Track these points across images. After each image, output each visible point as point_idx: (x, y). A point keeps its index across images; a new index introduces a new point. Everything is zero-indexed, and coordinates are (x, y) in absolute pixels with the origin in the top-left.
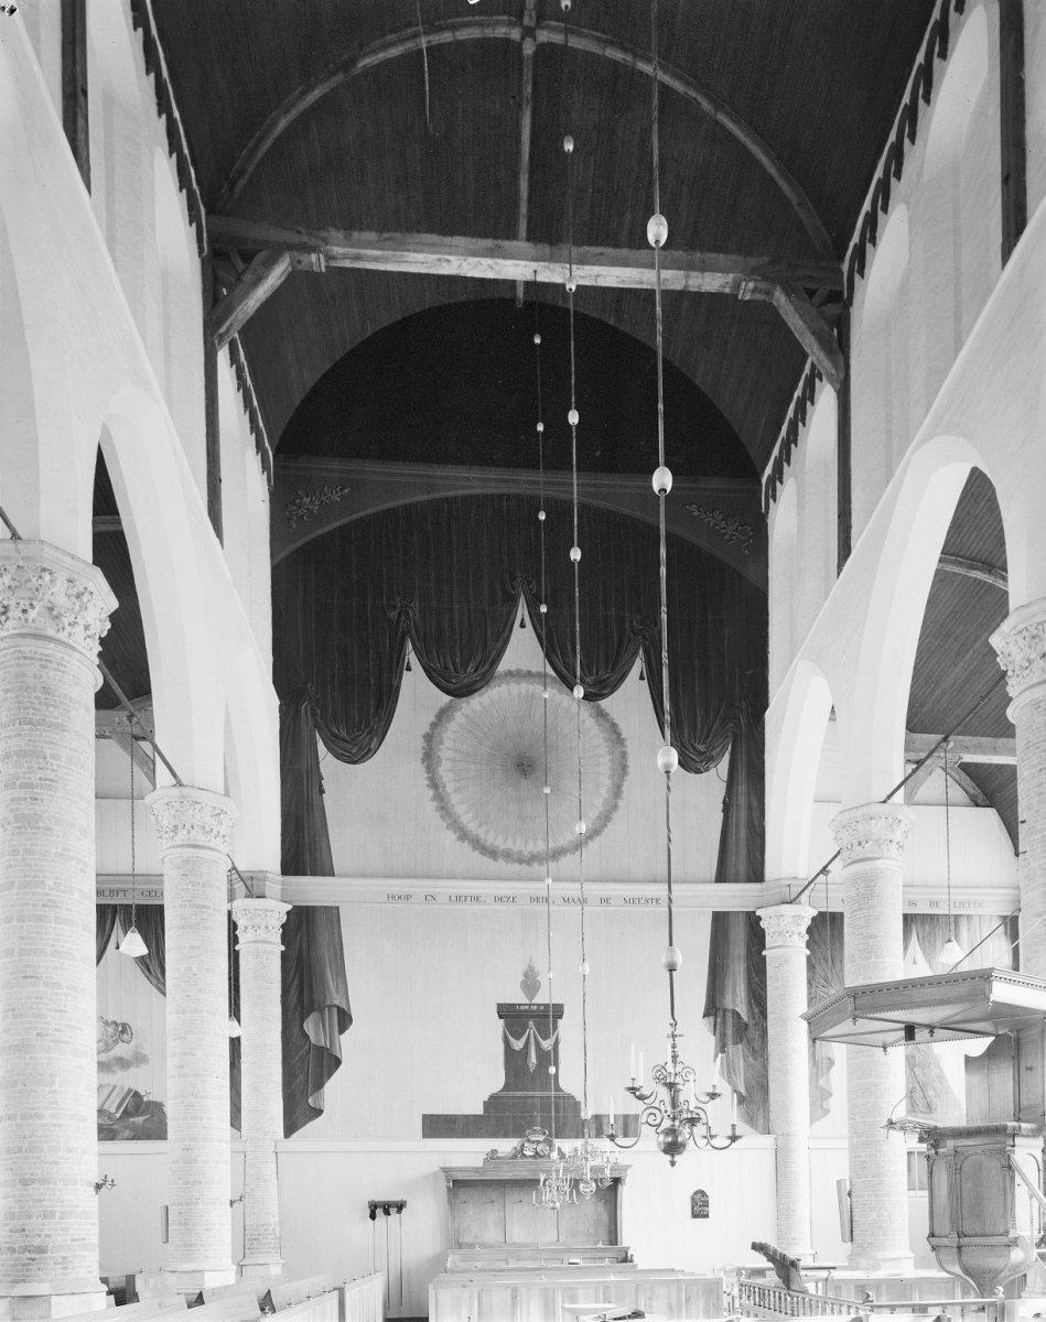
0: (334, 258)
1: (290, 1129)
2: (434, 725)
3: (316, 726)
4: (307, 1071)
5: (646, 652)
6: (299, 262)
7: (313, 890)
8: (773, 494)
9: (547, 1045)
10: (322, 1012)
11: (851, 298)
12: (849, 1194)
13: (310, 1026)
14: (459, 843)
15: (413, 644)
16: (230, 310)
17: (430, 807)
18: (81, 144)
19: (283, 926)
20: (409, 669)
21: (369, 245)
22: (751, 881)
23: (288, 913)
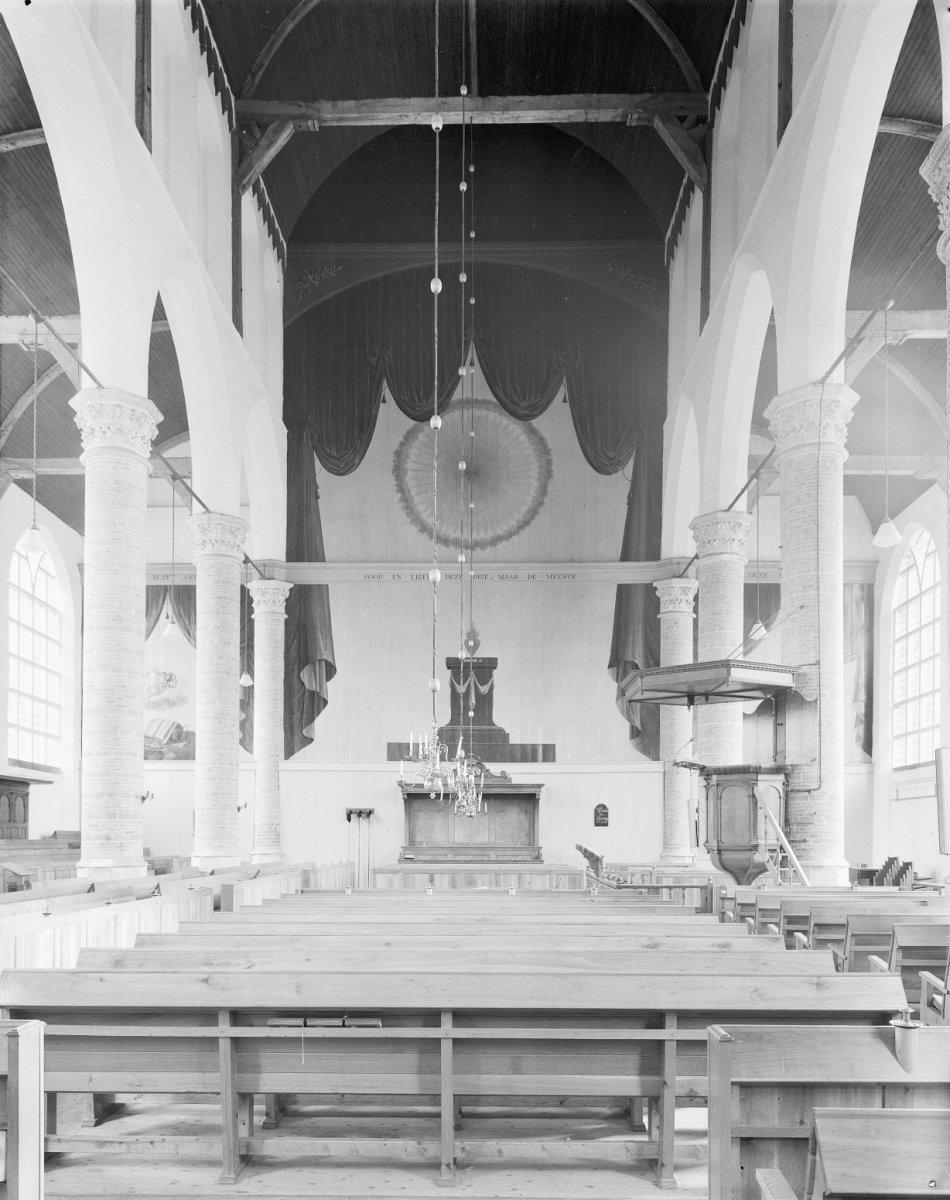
0: (325, 121)
1: (289, 752)
2: (402, 444)
3: (315, 448)
4: (302, 708)
5: (568, 380)
6: (300, 126)
7: (310, 573)
8: (671, 254)
9: (484, 689)
10: (314, 663)
11: (713, 121)
12: (697, 811)
13: (305, 675)
14: (420, 534)
15: (388, 382)
16: (250, 167)
17: (398, 508)
18: (146, 127)
19: (286, 600)
20: (384, 401)
21: (349, 110)
22: (650, 560)
23: (291, 590)
